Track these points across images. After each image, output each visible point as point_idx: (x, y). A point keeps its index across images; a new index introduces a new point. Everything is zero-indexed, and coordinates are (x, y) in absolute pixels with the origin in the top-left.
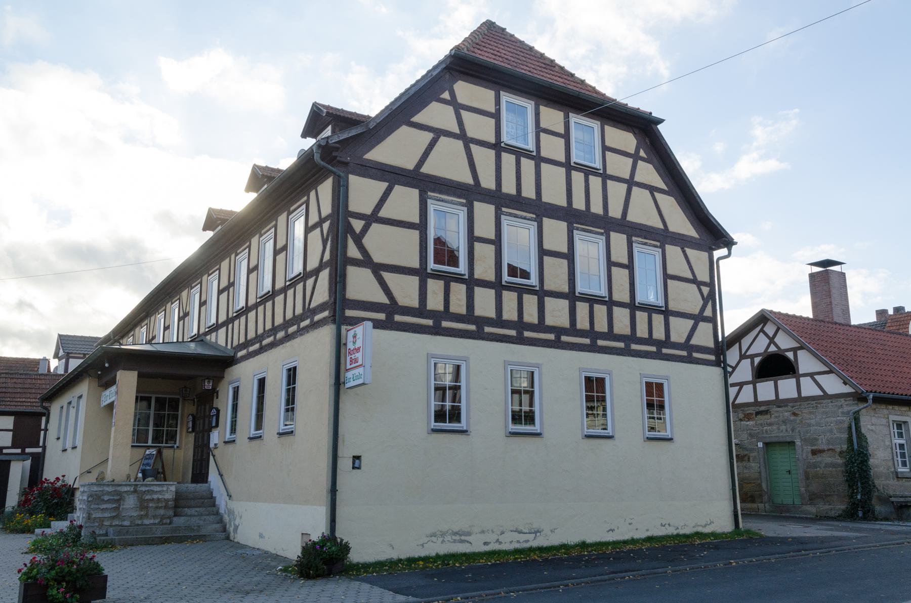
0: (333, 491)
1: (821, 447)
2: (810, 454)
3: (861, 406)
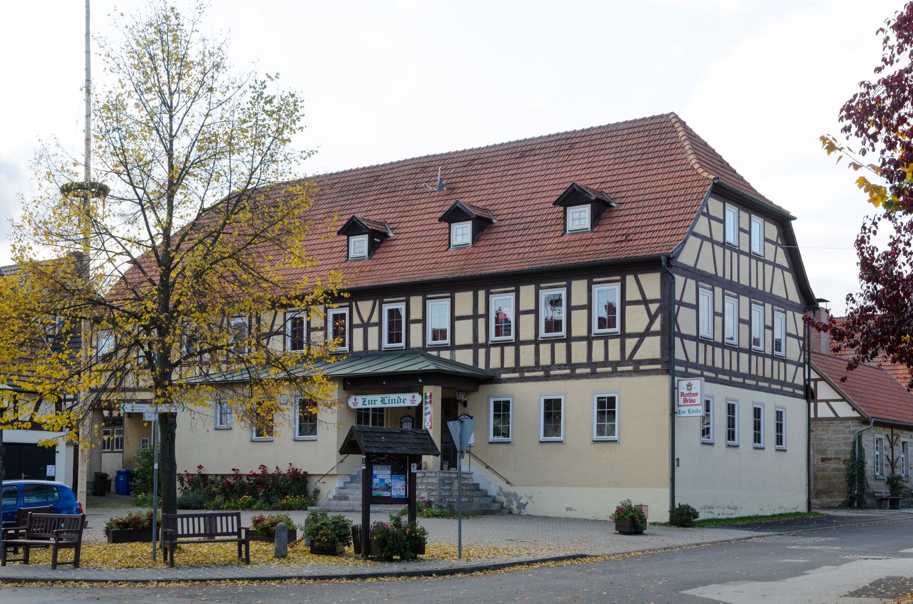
0: (673, 479)
1: (829, 456)
2: (820, 462)
3: (865, 427)
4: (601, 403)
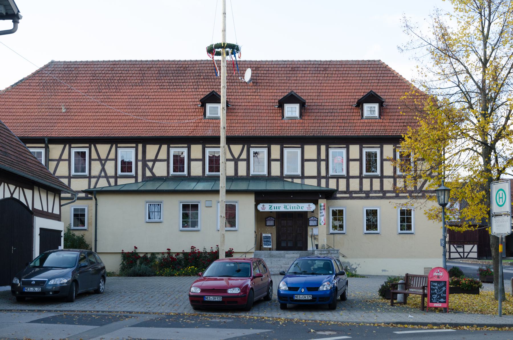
4: (402, 213)
